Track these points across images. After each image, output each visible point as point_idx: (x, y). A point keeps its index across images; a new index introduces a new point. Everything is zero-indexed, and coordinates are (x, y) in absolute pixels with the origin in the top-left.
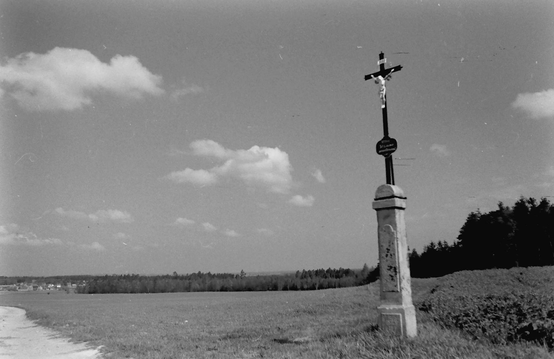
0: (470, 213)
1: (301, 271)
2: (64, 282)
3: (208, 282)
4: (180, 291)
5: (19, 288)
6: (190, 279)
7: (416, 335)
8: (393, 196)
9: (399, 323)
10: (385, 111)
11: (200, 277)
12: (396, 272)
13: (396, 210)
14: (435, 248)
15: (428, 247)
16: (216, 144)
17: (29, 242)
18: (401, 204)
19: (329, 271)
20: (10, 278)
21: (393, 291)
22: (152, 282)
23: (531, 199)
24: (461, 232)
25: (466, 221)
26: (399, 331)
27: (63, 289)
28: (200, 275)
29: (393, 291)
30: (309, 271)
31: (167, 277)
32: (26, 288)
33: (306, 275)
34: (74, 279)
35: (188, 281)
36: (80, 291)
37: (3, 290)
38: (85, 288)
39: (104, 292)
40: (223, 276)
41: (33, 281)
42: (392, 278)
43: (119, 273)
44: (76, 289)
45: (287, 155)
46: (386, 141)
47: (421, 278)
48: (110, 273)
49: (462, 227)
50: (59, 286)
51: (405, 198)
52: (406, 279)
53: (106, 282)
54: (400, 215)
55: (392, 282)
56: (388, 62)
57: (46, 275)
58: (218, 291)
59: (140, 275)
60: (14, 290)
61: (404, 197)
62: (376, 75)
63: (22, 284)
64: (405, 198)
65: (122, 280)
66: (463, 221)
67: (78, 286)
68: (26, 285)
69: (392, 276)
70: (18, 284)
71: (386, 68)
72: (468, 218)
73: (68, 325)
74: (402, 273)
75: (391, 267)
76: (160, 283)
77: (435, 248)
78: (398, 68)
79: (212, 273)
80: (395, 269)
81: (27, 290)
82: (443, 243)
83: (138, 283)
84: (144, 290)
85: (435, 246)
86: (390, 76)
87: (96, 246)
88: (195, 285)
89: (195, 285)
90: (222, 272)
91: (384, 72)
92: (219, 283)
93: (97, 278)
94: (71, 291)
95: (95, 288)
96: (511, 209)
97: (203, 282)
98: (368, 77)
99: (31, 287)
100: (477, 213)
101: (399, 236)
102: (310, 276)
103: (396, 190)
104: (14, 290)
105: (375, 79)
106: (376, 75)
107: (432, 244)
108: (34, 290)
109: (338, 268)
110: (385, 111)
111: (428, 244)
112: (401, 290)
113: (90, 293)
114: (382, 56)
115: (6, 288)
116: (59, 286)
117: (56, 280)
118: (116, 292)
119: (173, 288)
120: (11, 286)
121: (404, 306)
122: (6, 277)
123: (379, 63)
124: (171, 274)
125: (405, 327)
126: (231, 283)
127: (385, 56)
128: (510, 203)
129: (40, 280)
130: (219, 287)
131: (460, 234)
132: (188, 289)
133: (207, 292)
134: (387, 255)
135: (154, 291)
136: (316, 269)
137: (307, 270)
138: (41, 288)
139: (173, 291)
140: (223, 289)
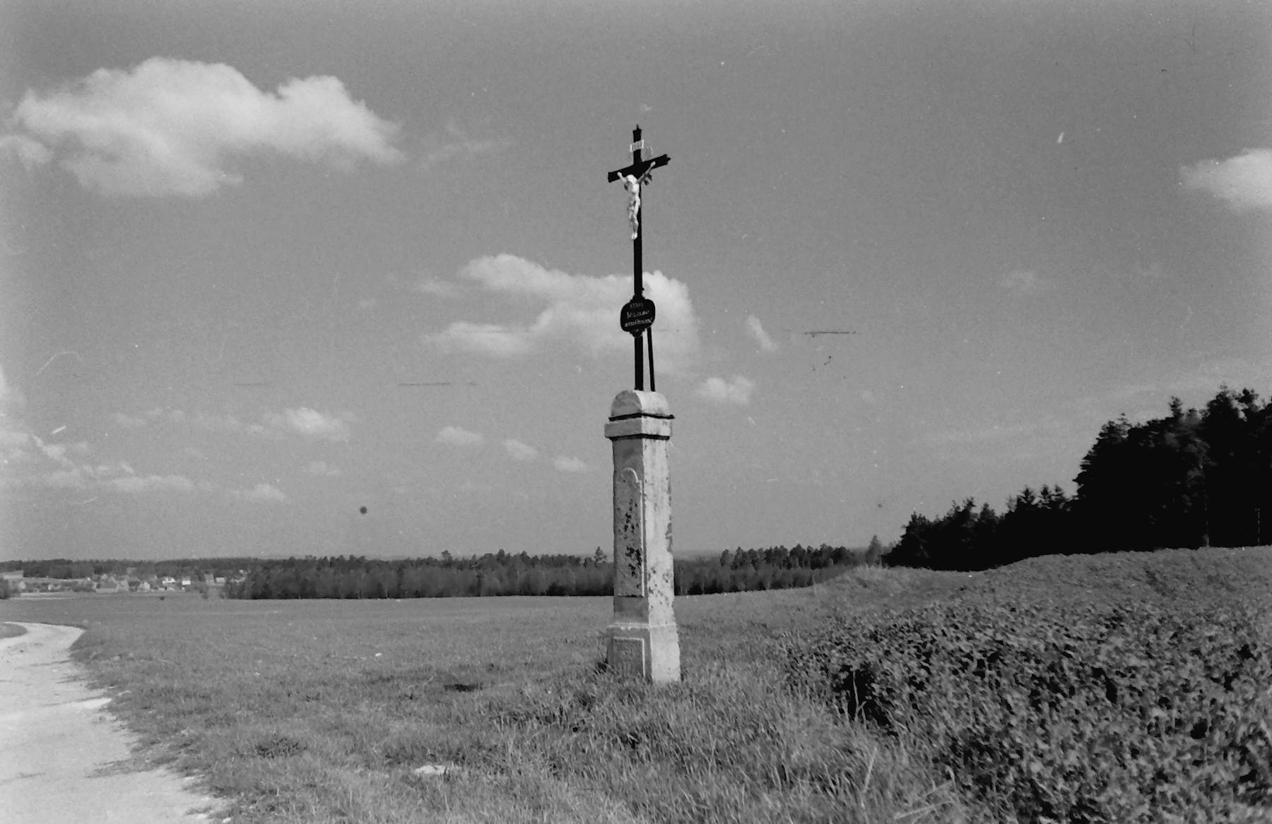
0: (1105, 422)
1: (733, 550)
2: (198, 573)
3: (521, 575)
4: (457, 595)
5: (98, 587)
6: (479, 567)
7: (676, 676)
8: (639, 414)
9: (640, 656)
10: (638, 244)
11: (503, 564)
12: (639, 559)
13: (645, 442)
14: (1036, 501)
15: (1019, 500)
16: (521, 263)
17: (159, 478)
18: (659, 430)
19: (797, 551)
20: (78, 563)
21: (634, 596)
22: (393, 573)
23: (1245, 391)
24: (1083, 466)
25: (1096, 442)
26: (641, 669)
27: (196, 588)
28: (502, 558)
29: (634, 596)
30: (751, 551)
31: (429, 562)
32: (114, 586)
33: (745, 559)
34: (219, 567)
35: (475, 573)
36: (233, 593)
37: (62, 590)
38: (243, 585)
39: (286, 595)
40: (557, 562)
41: (130, 570)
42: (633, 571)
43: (318, 554)
44: (224, 589)
45: (684, 287)
46: (638, 305)
47: (960, 570)
48: (300, 554)
49: (1085, 454)
50: (186, 582)
51: (671, 417)
52: (660, 573)
53: (290, 573)
54: (654, 450)
55: (633, 579)
56: (649, 149)
57: (158, 557)
58: (542, 594)
59: (369, 558)
60: (88, 589)
61: (668, 414)
62: (626, 172)
63: (104, 576)
64: (671, 417)
65: (326, 569)
66: (1089, 441)
67: (228, 583)
68: (113, 579)
69: (633, 568)
70: (96, 576)
71: (644, 158)
72: (1101, 434)
73: (117, 658)
74: (651, 562)
75: (632, 551)
76: (412, 575)
77: (1036, 501)
78: (662, 161)
79: (530, 554)
80: (638, 554)
81: (116, 590)
82: (1052, 491)
83: (364, 575)
84: (377, 593)
85: (1033, 498)
86: (650, 177)
87: (266, 491)
88: (491, 579)
89: (491, 579)
90: (554, 552)
91: (639, 168)
92: (545, 577)
93: (269, 565)
94: (213, 593)
95: (266, 586)
96: (1199, 416)
97: (509, 574)
98: (613, 177)
99: (125, 583)
100: (1120, 423)
101: (648, 490)
102: (753, 562)
103: (647, 400)
104: (88, 589)
105: (624, 180)
106: (626, 172)
107: (1027, 492)
108: (132, 590)
109: (816, 546)
110: (638, 244)
111: (1017, 492)
112: (647, 595)
113: (255, 598)
114: (637, 135)
115: (66, 584)
116: (186, 582)
117: (180, 567)
118: (312, 595)
119: (441, 587)
120: (80, 581)
121: (650, 626)
122: (69, 562)
123: (631, 148)
124: (438, 556)
125: (649, 663)
126: (573, 577)
127: (643, 135)
128: (1197, 401)
129: (143, 569)
130: (545, 587)
131: (1080, 471)
132: (475, 590)
133: (517, 598)
134: (626, 527)
135: (397, 595)
136: (766, 547)
137: (746, 549)
138: (146, 586)
139: (440, 595)
140: (555, 591)
